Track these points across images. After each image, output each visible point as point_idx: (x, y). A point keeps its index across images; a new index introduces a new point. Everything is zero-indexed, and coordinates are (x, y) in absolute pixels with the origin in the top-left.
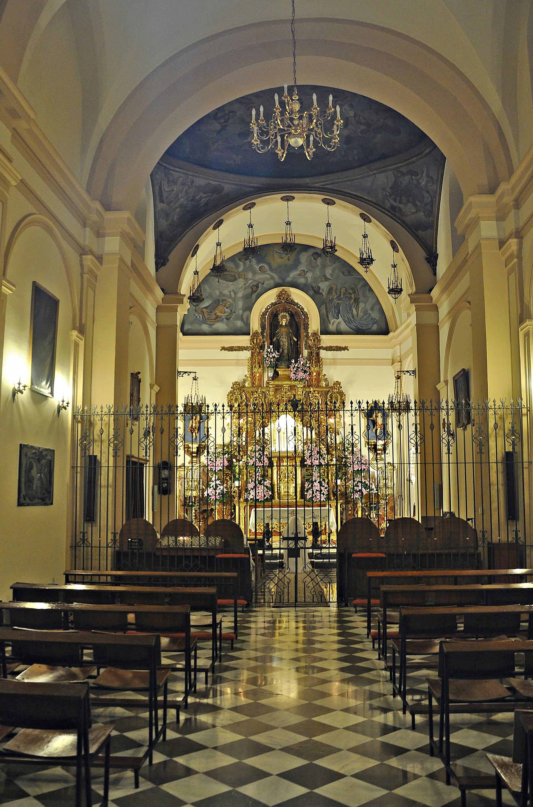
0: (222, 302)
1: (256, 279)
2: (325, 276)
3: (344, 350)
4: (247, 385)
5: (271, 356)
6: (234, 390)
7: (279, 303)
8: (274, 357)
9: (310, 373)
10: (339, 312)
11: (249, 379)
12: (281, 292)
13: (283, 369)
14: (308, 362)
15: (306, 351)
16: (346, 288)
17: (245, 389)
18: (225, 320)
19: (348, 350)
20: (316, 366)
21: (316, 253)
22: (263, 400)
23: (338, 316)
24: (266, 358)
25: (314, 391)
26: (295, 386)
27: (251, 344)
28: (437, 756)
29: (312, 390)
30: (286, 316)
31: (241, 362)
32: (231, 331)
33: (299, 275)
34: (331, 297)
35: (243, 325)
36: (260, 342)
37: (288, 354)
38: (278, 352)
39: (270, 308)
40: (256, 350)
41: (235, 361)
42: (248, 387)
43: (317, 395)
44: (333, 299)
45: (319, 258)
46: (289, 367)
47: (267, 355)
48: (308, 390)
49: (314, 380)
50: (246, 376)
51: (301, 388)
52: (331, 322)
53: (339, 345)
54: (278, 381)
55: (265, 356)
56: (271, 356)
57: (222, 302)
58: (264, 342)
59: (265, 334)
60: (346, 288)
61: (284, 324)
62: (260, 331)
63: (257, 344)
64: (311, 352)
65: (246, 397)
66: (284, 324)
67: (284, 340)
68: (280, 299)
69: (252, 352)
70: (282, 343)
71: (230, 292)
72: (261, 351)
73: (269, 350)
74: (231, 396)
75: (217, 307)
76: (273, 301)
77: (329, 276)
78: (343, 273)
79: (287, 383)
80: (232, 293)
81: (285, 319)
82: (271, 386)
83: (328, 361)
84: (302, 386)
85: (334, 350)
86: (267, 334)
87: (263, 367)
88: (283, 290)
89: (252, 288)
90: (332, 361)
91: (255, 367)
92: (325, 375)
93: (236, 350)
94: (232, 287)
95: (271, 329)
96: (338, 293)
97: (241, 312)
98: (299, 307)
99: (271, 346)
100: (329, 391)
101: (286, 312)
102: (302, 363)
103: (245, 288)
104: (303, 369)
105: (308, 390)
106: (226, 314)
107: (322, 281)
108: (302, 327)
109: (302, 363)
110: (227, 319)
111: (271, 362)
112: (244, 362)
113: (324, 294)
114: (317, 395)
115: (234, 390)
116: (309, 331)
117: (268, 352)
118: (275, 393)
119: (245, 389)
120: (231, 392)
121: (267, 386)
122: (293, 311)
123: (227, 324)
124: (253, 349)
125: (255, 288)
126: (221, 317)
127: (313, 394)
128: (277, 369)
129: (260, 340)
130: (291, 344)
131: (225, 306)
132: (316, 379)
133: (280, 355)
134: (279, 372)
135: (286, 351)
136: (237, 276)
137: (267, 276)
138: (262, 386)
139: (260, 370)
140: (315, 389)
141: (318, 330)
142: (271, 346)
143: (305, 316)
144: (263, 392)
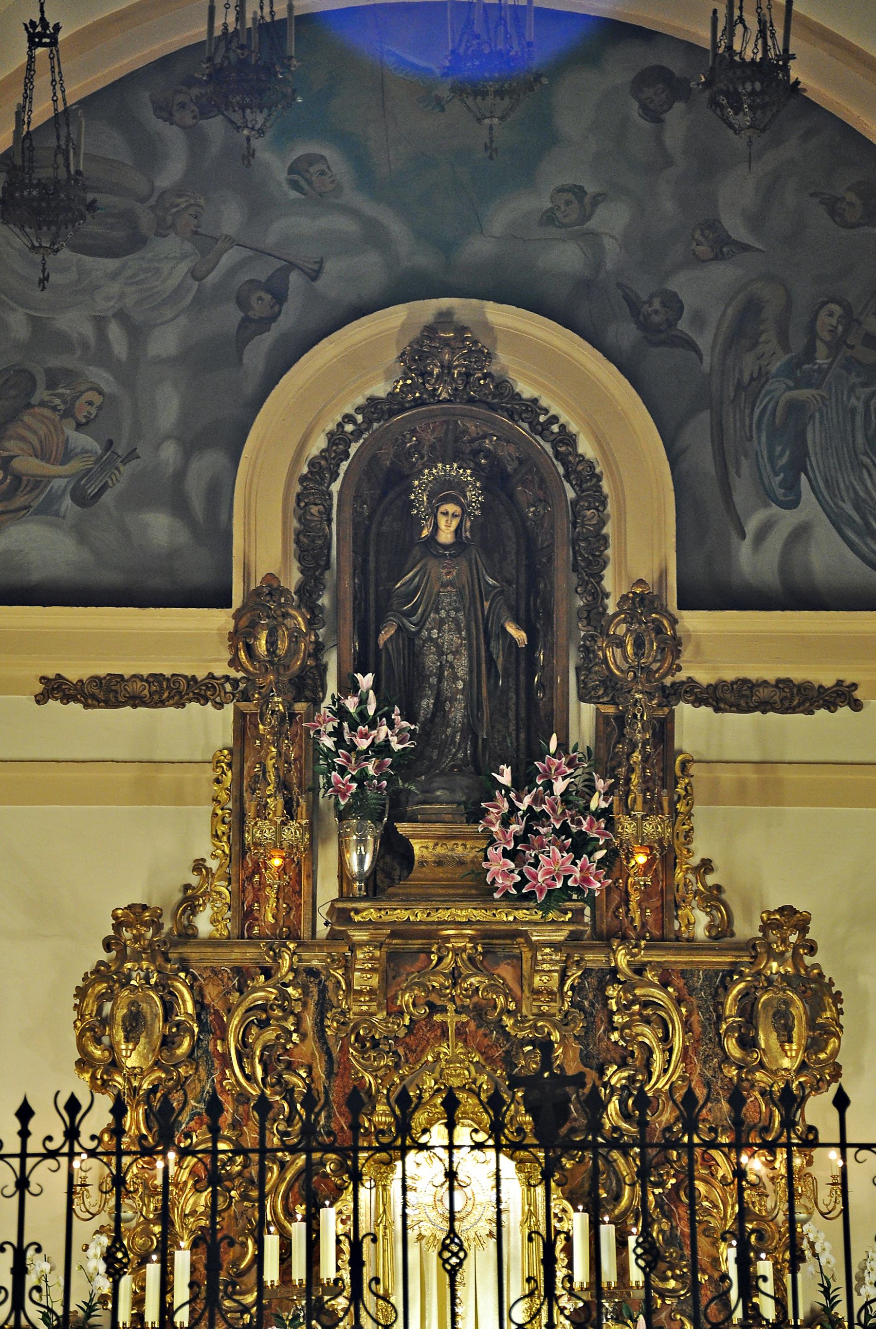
0: (51, 385)
1: (271, 239)
2: (712, 225)
3: (831, 706)
4: (203, 924)
5: (363, 744)
6: (122, 958)
7: (418, 403)
8: (381, 749)
9: (613, 854)
10: (799, 465)
11: (222, 887)
12: (430, 331)
13: (439, 828)
14: (600, 784)
15: (588, 710)
16: (848, 309)
17: (192, 953)
18: (68, 502)
19: (856, 706)
20: (652, 808)
21: (661, 75)
22: (309, 1022)
23: (792, 486)
24: (329, 754)
25: (639, 970)
26: (514, 935)
27: (234, 662)
28: (191, 1293)
29: (622, 959)
30: (461, 487)
31: (167, 774)
32: (109, 578)
33: (549, 218)
34: (749, 364)
35: (183, 537)
36: (292, 652)
37: (470, 729)
38: (409, 716)
39: (357, 434)
40: (266, 700)
41: (127, 773)
42: (212, 942)
43: (658, 994)
44: (761, 377)
45: (679, 106)
46: (476, 815)
47: (337, 733)
48: (594, 959)
49: (635, 897)
50: (199, 866)
51: (556, 946)
52: (751, 526)
53: (798, 674)
54: (408, 901)
55: (328, 742)
56: (363, 744)
57: (51, 385)
58: (318, 649)
59: (325, 600)
60: (848, 309)
61: (446, 536)
62: (293, 579)
63: (273, 660)
64: (620, 719)
65: (200, 1005)
66: (446, 536)
67: (450, 638)
68: (424, 374)
69: (240, 716)
70: (431, 661)
71: (100, 322)
72: (300, 707)
73: (351, 704)
74: (101, 998)
75: (14, 416)
76: (381, 390)
77: (737, 230)
78: (833, 207)
79: (462, 914)
80: (115, 332)
81: (451, 508)
82: (359, 936)
83: (726, 775)
84: (560, 936)
85: (765, 707)
86: (337, 601)
87: (314, 810)
88: (445, 318)
89: (242, 302)
90: (750, 774)
91: (262, 812)
92: (706, 866)
93: (136, 701)
94: (115, 288)
95: (361, 569)
96: (798, 342)
97: (170, 452)
98: (543, 430)
99: (366, 681)
100: (734, 969)
101: (457, 456)
102: (560, 786)
103: (200, 302)
104: (565, 830)
105: (594, 959)
106: (75, 466)
107: (696, 261)
108: (563, 556)
109: (560, 786)
110: (82, 499)
111: (362, 778)
112: (190, 774)
113: (704, 341)
114: (658, 994)
115: (122, 958)
116: (608, 584)
117: (341, 713)
118: (386, 982)
119: (192, 953)
120: (100, 972)
121: (333, 936)
122: (507, 452)
123: (82, 539)
124: (246, 697)
125: (261, 302)
126: (38, 483)
127: (628, 986)
128: (403, 828)
129: (295, 637)
130: (491, 662)
131: (68, 413)
132: (647, 893)
133: (423, 738)
134: (417, 847)
135: (457, 713)
136: (146, 219)
137: (345, 225)
138: (305, 932)
139: (292, 833)
140: (643, 957)
141: (663, 575)
142: (366, 681)
143: (579, 486)
144: (312, 972)
